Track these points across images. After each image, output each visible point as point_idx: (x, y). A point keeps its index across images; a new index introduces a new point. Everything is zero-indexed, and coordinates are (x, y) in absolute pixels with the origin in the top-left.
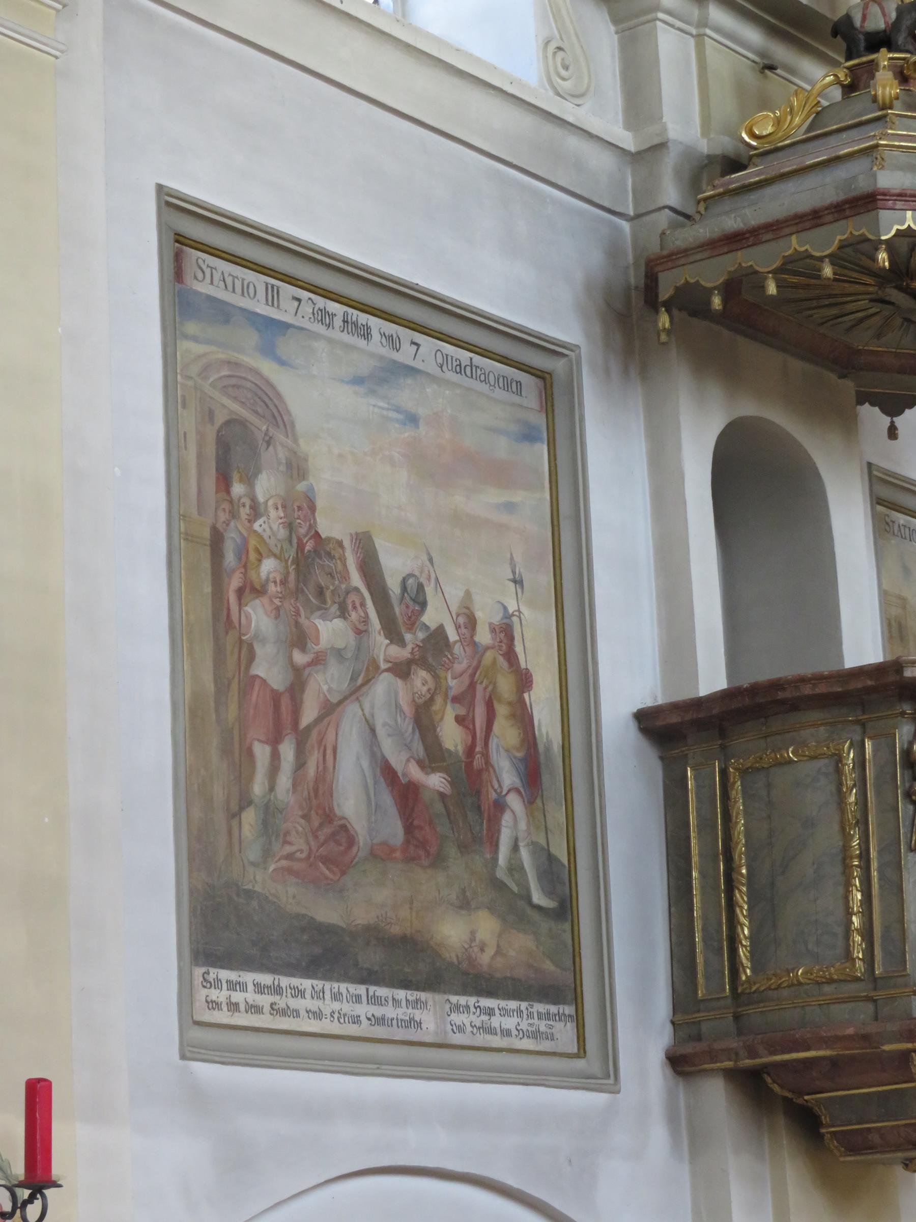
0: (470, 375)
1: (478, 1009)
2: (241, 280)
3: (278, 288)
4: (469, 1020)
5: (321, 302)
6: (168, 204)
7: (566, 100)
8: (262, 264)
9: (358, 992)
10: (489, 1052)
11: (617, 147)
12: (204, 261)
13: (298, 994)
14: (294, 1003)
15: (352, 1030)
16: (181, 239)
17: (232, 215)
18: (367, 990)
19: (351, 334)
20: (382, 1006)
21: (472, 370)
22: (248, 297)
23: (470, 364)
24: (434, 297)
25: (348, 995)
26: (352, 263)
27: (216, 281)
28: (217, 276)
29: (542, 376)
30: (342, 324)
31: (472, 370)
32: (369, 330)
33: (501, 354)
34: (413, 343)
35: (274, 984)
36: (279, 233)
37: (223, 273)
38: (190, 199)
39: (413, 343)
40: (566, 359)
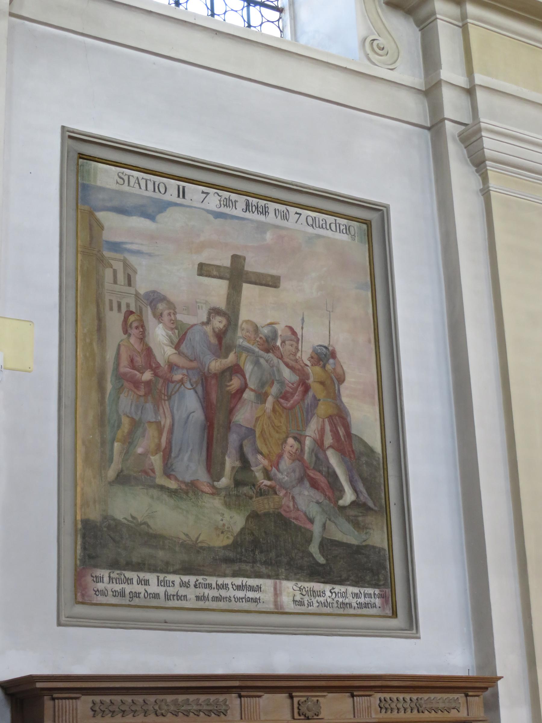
0: (335, 230)
1: (334, 594)
2: (153, 182)
3: (184, 188)
4: (316, 600)
5: (226, 194)
6: (70, 137)
7: (377, 65)
8: (228, 187)
9: (369, 592)
10: (234, 613)
11: (414, 88)
12: (123, 173)
13: (126, 582)
14: (182, 591)
15: (328, 610)
16: (81, 156)
17: (100, 137)
18: (158, 577)
19: (251, 212)
20: (321, 596)
21: (336, 226)
22: (330, 230)
23: (334, 222)
24: (310, 189)
25: (139, 580)
26: (213, 164)
27: (132, 184)
28: (132, 181)
29: (368, 223)
30: (245, 208)
31: (336, 226)
32: (267, 209)
33: (364, 219)
34: (296, 213)
35: (242, 584)
36: (276, 178)
37: (137, 178)
38: (199, 160)
39: (296, 213)
40: (380, 213)
